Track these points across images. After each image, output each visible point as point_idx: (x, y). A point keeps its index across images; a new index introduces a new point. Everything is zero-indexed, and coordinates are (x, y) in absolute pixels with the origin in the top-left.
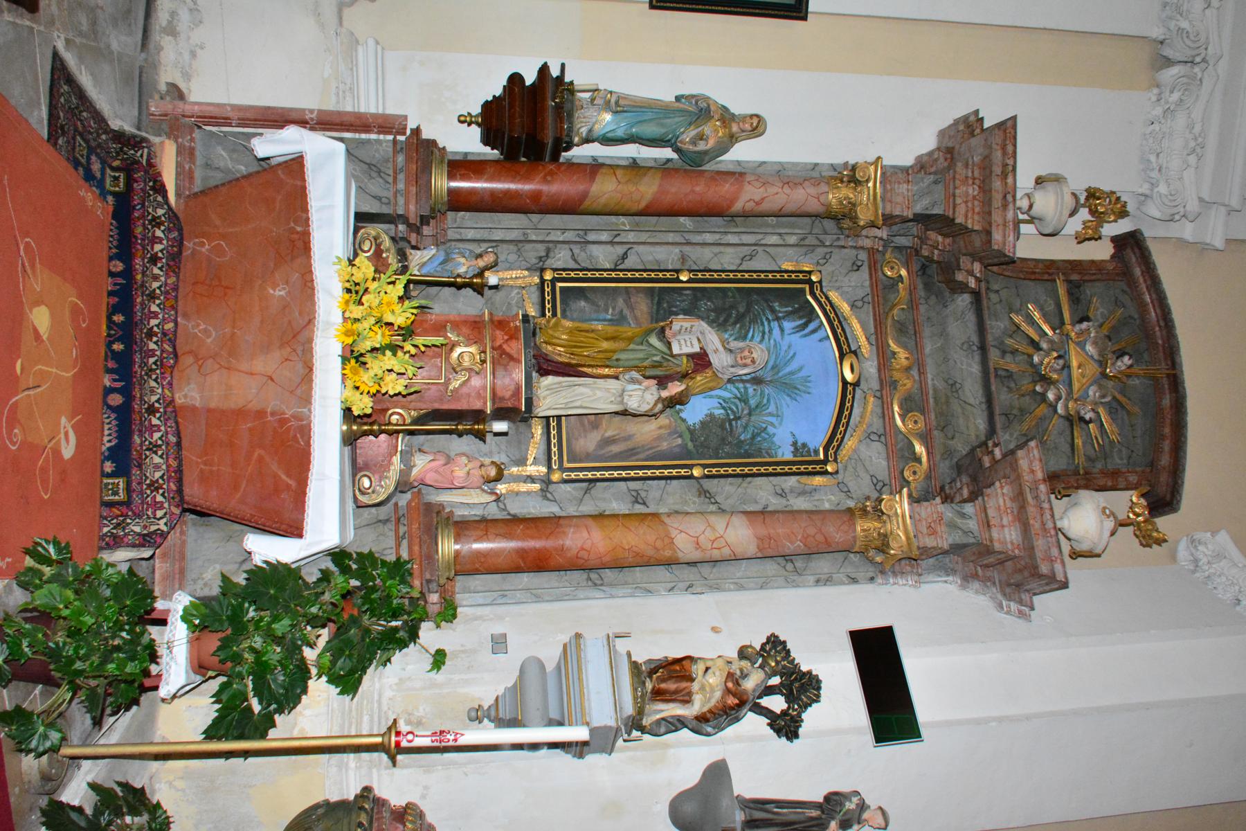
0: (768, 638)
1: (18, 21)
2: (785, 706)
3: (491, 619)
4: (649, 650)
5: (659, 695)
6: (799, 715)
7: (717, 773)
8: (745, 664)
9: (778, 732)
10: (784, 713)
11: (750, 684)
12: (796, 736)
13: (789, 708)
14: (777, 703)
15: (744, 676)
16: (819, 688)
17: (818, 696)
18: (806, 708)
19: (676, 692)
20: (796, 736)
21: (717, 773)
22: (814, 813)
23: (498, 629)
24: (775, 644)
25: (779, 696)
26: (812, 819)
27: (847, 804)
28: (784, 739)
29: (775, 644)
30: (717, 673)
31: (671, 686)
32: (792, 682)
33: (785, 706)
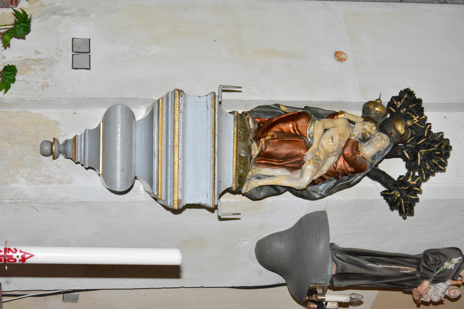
0: (402, 93)
1: (5, 110)
2: (403, 171)
3: (72, 15)
4: (259, 93)
5: (267, 158)
6: (418, 185)
7: (314, 224)
8: (370, 127)
9: (393, 205)
10: (402, 181)
11: (368, 151)
12: (411, 213)
13: (408, 174)
14: (396, 168)
15: (365, 139)
16: (447, 155)
17: (444, 165)
18: (428, 177)
19: (288, 157)
20: (411, 213)
21: (314, 224)
22: (409, 270)
23: (81, 32)
24: (408, 104)
25: (400, 160)
26: (407, 275)
27: (446, 264)
28: (396, 212)
29: (408, 104)
30: (336, 139)
31: (284, 150)
32: (418, 148)
33: (403, 171)
